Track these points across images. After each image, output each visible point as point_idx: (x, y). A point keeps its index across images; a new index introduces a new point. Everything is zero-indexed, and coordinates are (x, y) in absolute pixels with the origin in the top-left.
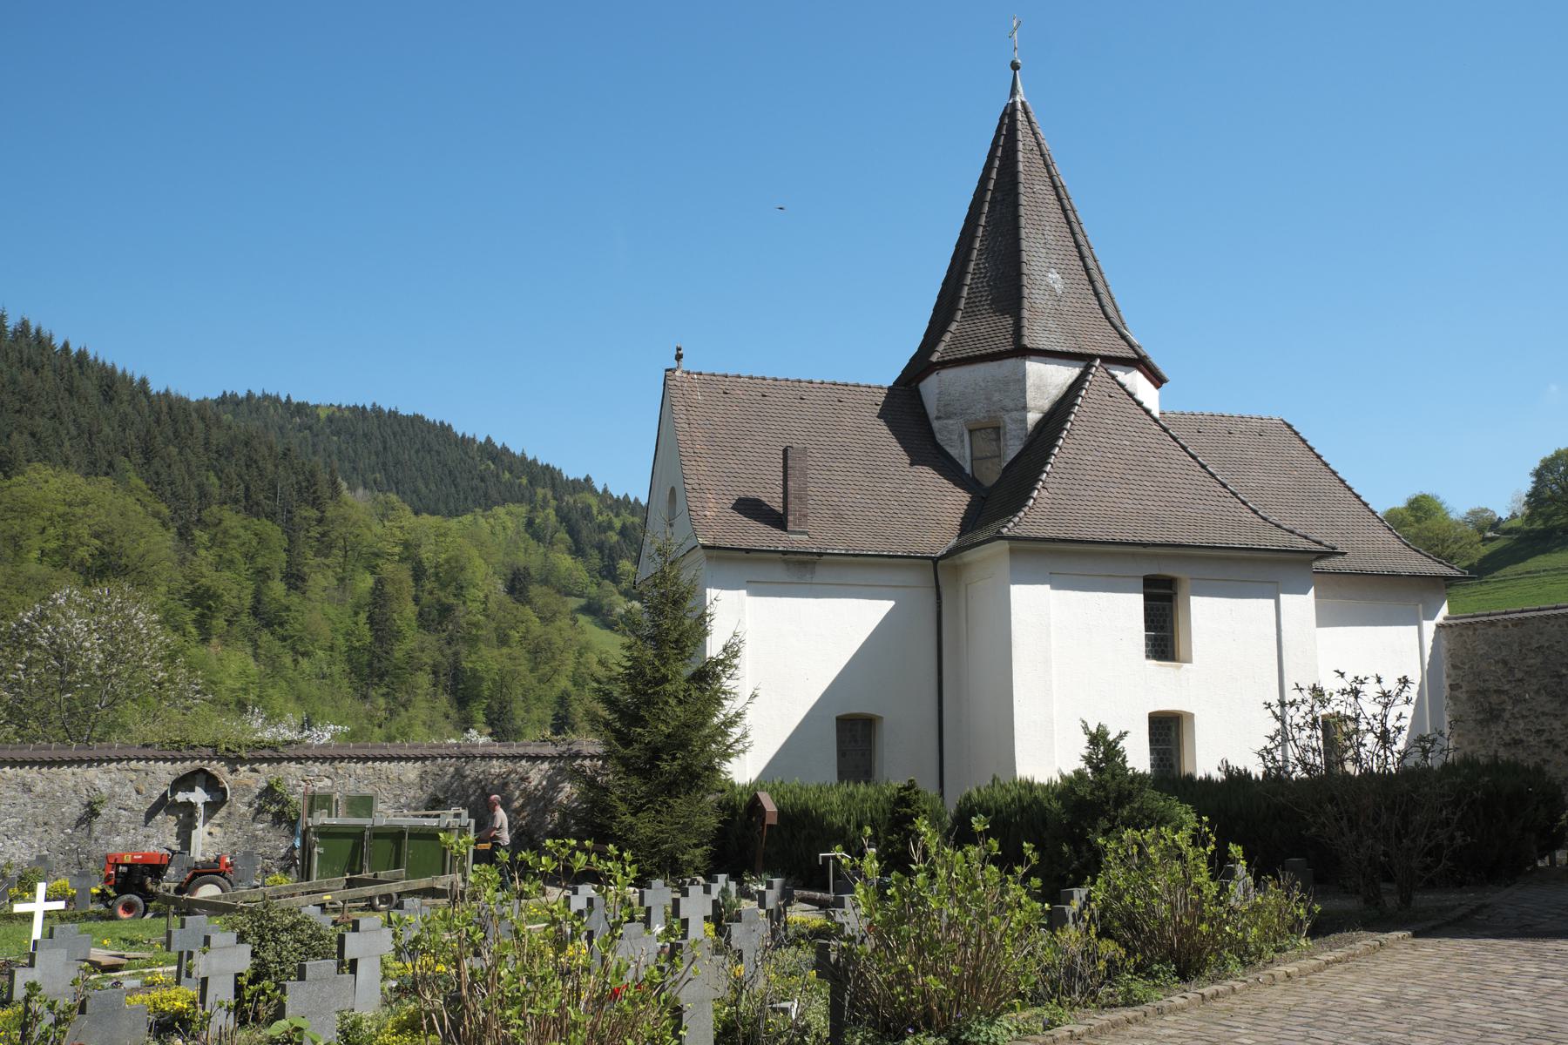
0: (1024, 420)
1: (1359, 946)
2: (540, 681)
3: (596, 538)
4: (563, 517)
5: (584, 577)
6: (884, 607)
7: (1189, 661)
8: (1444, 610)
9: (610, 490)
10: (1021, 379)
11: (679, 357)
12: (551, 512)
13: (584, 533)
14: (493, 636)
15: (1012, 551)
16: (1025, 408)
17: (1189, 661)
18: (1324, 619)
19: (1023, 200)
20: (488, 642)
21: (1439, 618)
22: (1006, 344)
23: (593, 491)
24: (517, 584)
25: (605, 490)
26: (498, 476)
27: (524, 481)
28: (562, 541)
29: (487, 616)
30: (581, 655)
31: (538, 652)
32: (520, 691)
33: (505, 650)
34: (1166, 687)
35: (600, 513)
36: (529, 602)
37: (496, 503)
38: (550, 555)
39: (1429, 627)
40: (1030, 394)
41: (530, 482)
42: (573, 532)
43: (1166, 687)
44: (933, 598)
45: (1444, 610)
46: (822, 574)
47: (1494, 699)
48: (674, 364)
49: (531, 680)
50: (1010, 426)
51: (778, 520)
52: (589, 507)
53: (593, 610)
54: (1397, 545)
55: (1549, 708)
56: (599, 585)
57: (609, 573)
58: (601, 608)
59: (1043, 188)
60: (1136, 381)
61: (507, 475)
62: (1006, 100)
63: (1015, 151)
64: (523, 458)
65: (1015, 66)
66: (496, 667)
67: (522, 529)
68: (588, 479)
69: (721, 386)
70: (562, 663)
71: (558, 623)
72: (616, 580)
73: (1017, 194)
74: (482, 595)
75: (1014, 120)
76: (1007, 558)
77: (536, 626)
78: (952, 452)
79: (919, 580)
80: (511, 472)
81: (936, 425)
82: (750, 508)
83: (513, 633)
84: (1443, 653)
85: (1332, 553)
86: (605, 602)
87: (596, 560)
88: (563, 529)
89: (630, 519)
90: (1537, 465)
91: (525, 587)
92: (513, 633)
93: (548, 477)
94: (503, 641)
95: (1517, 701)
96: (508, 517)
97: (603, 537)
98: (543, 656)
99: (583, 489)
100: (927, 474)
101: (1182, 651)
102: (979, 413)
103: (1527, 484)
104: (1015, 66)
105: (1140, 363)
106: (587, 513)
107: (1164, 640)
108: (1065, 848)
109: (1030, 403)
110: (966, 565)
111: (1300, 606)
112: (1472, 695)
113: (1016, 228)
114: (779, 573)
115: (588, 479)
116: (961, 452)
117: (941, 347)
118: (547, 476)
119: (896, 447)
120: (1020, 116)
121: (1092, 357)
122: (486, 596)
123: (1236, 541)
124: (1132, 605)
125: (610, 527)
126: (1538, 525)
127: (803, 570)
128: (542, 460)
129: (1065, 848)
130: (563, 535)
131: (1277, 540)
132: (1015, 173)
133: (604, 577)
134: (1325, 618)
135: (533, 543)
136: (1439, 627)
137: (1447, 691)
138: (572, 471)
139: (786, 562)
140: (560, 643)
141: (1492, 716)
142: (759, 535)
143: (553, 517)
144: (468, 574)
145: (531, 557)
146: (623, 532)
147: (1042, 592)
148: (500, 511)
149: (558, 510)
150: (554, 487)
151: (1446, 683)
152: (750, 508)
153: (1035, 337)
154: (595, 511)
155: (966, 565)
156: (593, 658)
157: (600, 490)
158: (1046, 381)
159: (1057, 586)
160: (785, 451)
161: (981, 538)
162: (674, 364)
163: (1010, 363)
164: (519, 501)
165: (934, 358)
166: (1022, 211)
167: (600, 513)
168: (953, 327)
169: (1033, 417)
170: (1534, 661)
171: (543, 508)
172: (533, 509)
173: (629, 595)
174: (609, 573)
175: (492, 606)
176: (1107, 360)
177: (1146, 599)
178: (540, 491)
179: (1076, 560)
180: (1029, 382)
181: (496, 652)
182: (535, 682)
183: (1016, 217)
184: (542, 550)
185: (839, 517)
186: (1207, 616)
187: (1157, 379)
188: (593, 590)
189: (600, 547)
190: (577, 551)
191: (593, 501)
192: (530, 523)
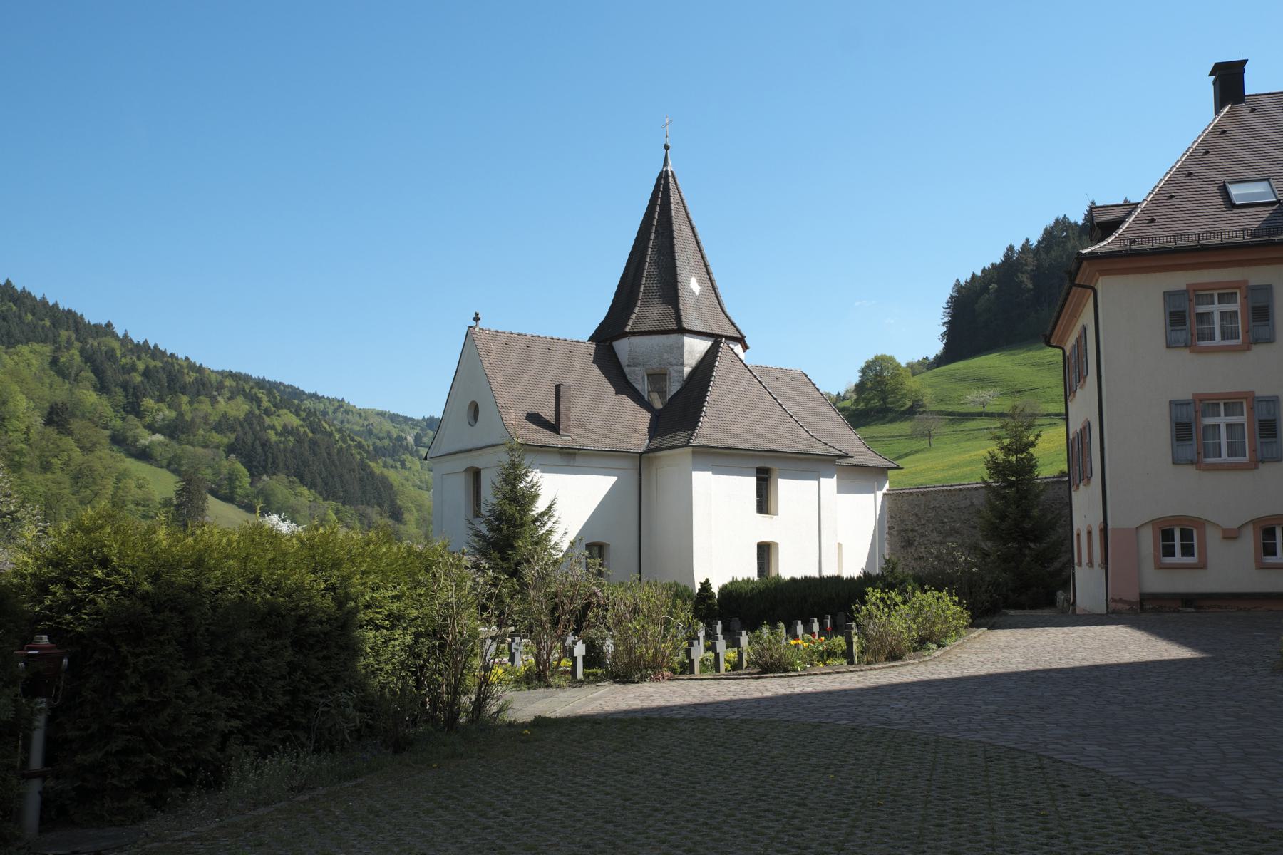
0: (682, 372)
1: (973, 635)
2: (81, 503)
3: (121, 378)
4: (88, 357)
5: (109, 412)
6: (613, 479)
7: (776, 514)
8: (887, 486)
9: (130, 335)
10: (681, 347)
11: (477, 319)
12: (75, 352)
13: (109, 373)
14: (37, 463)
15: (693, 453)
16: (682, 364)
17: (776, 514)
18: (841, 489)
19: (675, 234)
20: (30, 467)
21: (885, 490)
22: (672, 325)
23: (115, 336)
24: (57, 417)
25: (126, 336)
26: (20, 317)
27: (48, 323)
28: (86, 379)
29: (30, 445)
30: (119, 481)
31: (80, 478)
32: (63, 511)
33: (49, 476)
34: (765, 528)
35: (124, 356)
36: (70, 433)
37: (19, 342)
38: (76, 391)
39: (880, 494)
40: (685, 356)
41: (53, 324)
42: (97, 371)
43: (765, 528)
44: (484, 451)
45: (887, 486)
46: (579, 461)
47: (910, 534)
48: (474, 323)
49: (74, 501)
50: (674, 374)
51: (554, 428)
52: (113, 350)
53: (118, 440)
54: (863, 448)
55: (938, 539)
56: (123, 419)
57: (134, 408)
58: (125, 439)
59: (685, 228)
60: (738, 348)
61: (30, 317)
62: (659, 168)
63: (669, 203)
64: (44, 302)
65: (667, 147)
66: (42, 490)
67: (47, 366)
68: (109, 325)
69: (505, 340)
70: (104, 487)
71: (98, 453)
72: (139, 415)
73: (672, 231)
74: (23, 427)
75: (667, 183)
76: (690, 457)
77: (77, 454)
78: (637, 387)
79: (629, 466)
80: (33, 314)
81: (626, 370)
82: (534, 418)
83: (54, 460)
84: (886, 509)
85: (847, 456)
86: (129, 434)
87: (120, 397)
88: (88, 367)
89: (152, 363)
90: (863, 365)
91: (67, 421)
92: (54, 460)
93: (71, 321)
94: (46, 467)
95: (922, 536)
96: (32, 356)
97: (127, 377)
98: (83, 481)
99: (106, 334)
100: (625, 399)
101: (772, 508)
102: (655, 365)
103: (855, 378)
104: (667, 147)
105: (741, 340)
106: (111, 355)
107: (764, 505)
108: (65, 661)
109: (686, 362)
110: (656, 458)
111: (829, 484)
112: (899, 532)
113: (672, 253)
114: (556, 459)
115: (109, 325)
116: (643, 387)
117: (631, 322)
118: (71, 320)
119: (607, 383)
120: (671, 180)
121: (722, 336)
122: (28, 428)
123: (802, 449)
124: (751, 482)
125: (133, 368)
126: (862, 406)
127: (572, 459)
128: (64, 305)
129: (65, 661)
130: (88, 374)
131: (820, 449)
132: (670, 218)
133: (128, 413)
134: (841, 489)
135: (58, 380)
136: (885, 495)
137: (886, 530)
138: (93, 316)
139: (561, 453)
140: (102, 470)
141: (909, 543)
142: (543, 437)
143: (77, 358)
144: (11, 405)
145: (60, 392)
146: (146, 373)
147: (707, 475)
148: (24, 349)
149: (82, 352)
150: (77, 330)
151: (886, 525)
152: (534, 418)
153: (689, 323)
154: (119, 354)
155: (656, 458)
156: (131, 484)
157: (121, 335)
158: (695, 348)
159: (714, 473)
160: (558, 388)
161: (673, 443)
162: (474, 323)
163: (674, 337)
164: (44, 341)
165: (628, 329)
166: (676, 242)
167: (124, 356)
168: (636, 310)
169: (687, 370)
170: (931, 514)
171: (68, 349)
172: (57, 349)
173: (152, 429)
174: (134, 408)
175: (34, 435)
176: (728, 338)
177: (758, 479)
178: (64, 334)
179: (723, 458)
180: (685, 349)
181: (41, 477)
182: (76, 503)
183: (672, 246)
184: (67, 386)
185: (583, 426)
186: (788, 489)
187: (745, 348)
188: (118, 423)
189: (125, 386)
190: (102, 388)
191: (116, 345)
192: (54, 362)
